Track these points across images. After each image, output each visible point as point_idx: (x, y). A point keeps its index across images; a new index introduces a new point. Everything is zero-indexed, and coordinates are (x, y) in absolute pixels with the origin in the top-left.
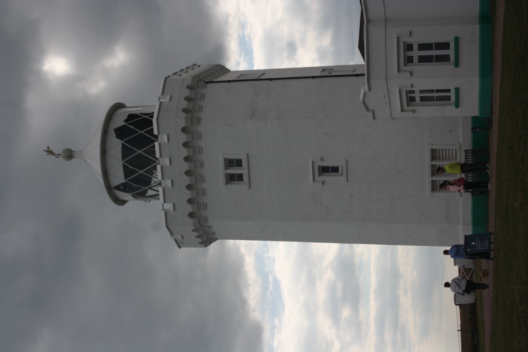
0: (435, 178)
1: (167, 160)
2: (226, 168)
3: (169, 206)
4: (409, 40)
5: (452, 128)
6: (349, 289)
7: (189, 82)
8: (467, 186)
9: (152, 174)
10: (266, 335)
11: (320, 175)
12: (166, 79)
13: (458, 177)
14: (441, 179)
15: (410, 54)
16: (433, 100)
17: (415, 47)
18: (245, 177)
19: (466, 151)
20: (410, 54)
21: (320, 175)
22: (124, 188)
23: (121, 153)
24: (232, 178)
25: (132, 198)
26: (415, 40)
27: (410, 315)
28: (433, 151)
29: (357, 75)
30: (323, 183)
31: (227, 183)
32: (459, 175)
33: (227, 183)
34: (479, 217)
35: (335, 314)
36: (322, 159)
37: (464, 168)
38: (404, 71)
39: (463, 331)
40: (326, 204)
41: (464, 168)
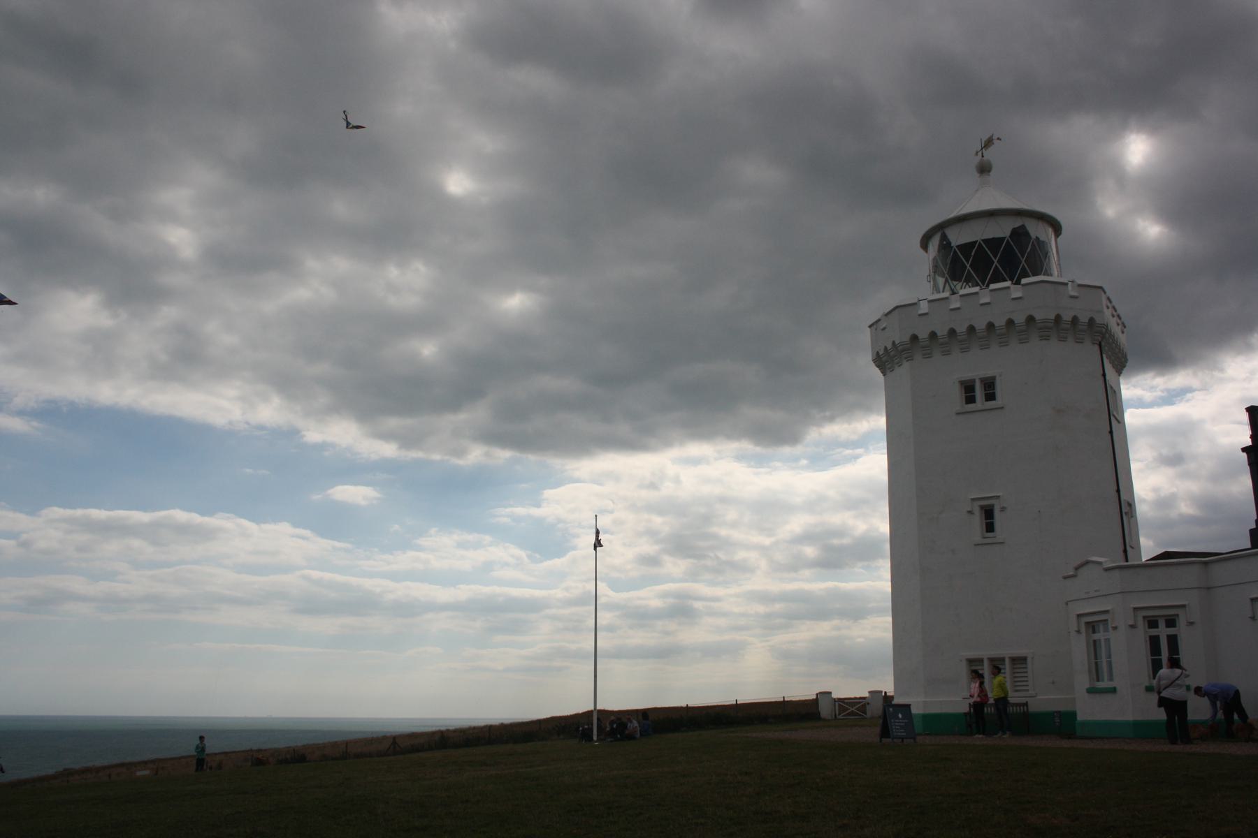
0: (986, 663)
1: (987, 300)
2: (982, 380)
3: (924, 307)
4: (1182, 622)
5: (1055, 682)
6: (837, 554)
7: (1098, 320)
8: (978, 707)
9: (967, 281)
10: (786, 450)
11: (982, 507)
12: (1101, 288)
13: (990, 695)
14: (986, 670)
15: (1162, 624)
16: (1096, 657)
17: (1171, 631)
18: (971, 407)
19: (1026, 704)
20: (1162, 624)
21: (982, 507)
22: (945, 245)
23: (991, 237)
24: (968, 390)
25: (931, 258)
26: (1182, 630)
27: (807, 634)
28: (1023, 660)
29: (1125, 551)
30: (970, 512)
31: (962, 383)
32: (992, 695)
33: (962, 383)
34: (936, 722)
35: (807, 537)
36: (1003, 509)
37: (1002, 702)
38: (1135, 616)
39: (784, 704)
40: (943, 520)
41: (1002, 702)
